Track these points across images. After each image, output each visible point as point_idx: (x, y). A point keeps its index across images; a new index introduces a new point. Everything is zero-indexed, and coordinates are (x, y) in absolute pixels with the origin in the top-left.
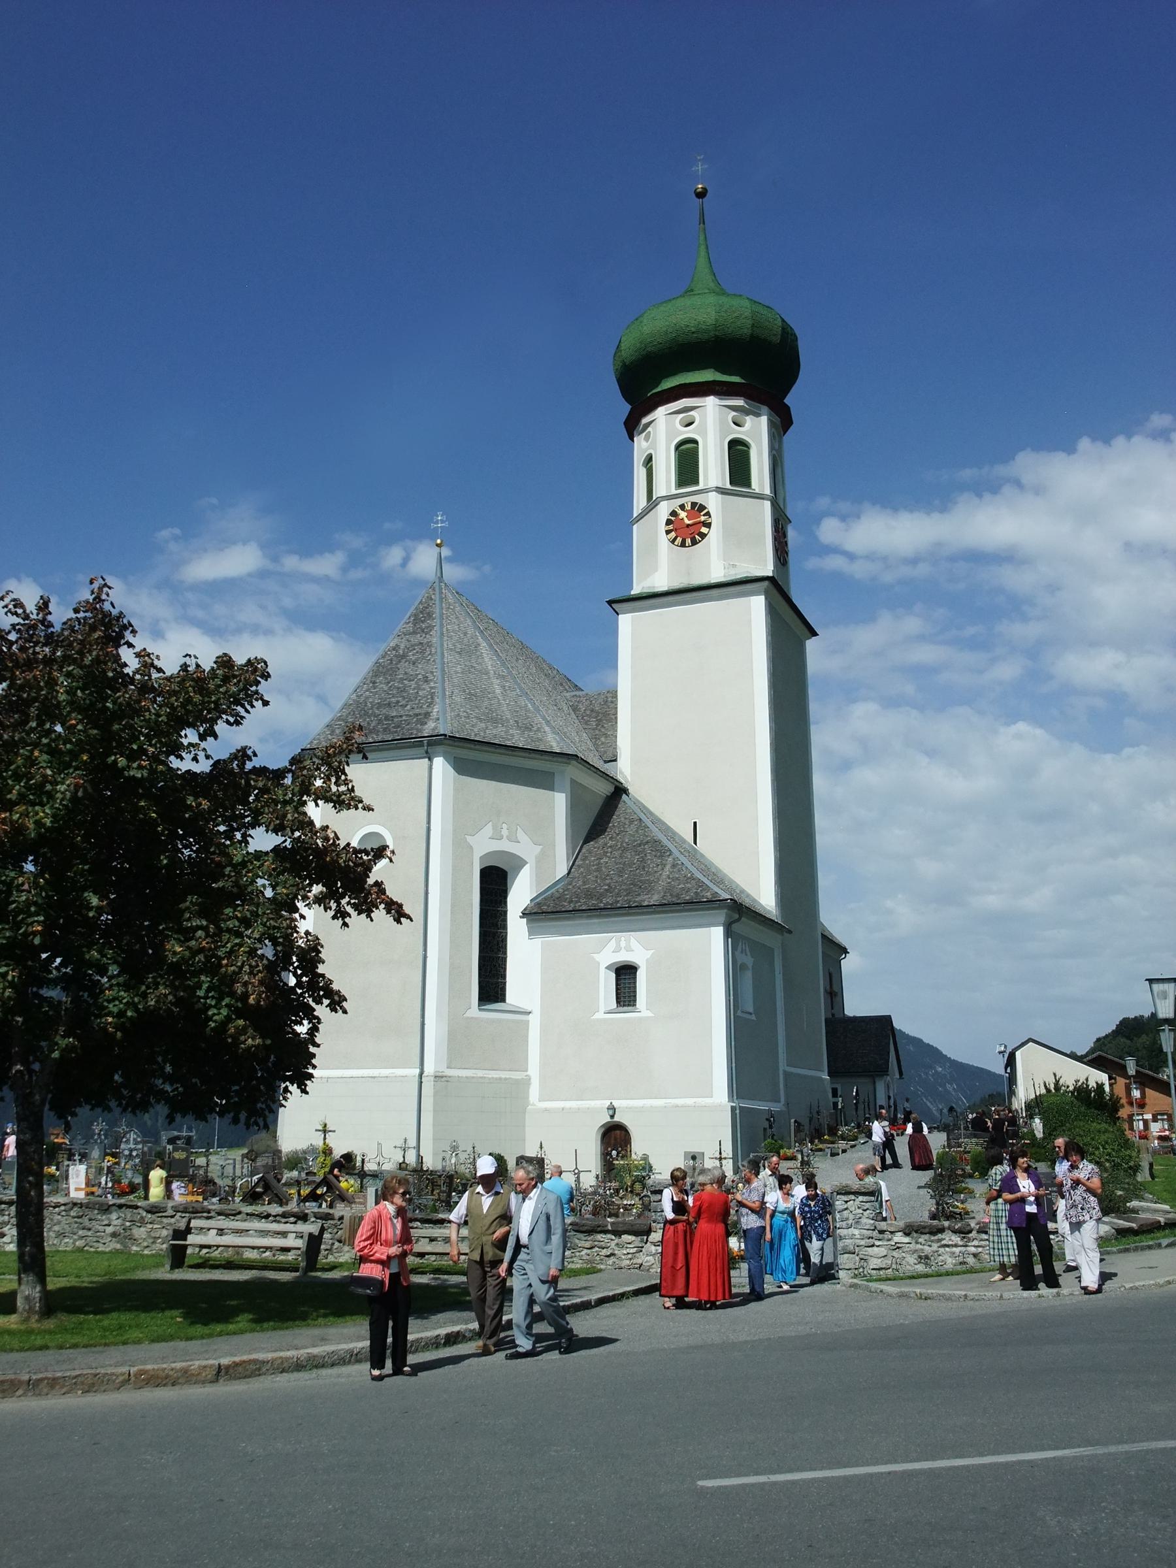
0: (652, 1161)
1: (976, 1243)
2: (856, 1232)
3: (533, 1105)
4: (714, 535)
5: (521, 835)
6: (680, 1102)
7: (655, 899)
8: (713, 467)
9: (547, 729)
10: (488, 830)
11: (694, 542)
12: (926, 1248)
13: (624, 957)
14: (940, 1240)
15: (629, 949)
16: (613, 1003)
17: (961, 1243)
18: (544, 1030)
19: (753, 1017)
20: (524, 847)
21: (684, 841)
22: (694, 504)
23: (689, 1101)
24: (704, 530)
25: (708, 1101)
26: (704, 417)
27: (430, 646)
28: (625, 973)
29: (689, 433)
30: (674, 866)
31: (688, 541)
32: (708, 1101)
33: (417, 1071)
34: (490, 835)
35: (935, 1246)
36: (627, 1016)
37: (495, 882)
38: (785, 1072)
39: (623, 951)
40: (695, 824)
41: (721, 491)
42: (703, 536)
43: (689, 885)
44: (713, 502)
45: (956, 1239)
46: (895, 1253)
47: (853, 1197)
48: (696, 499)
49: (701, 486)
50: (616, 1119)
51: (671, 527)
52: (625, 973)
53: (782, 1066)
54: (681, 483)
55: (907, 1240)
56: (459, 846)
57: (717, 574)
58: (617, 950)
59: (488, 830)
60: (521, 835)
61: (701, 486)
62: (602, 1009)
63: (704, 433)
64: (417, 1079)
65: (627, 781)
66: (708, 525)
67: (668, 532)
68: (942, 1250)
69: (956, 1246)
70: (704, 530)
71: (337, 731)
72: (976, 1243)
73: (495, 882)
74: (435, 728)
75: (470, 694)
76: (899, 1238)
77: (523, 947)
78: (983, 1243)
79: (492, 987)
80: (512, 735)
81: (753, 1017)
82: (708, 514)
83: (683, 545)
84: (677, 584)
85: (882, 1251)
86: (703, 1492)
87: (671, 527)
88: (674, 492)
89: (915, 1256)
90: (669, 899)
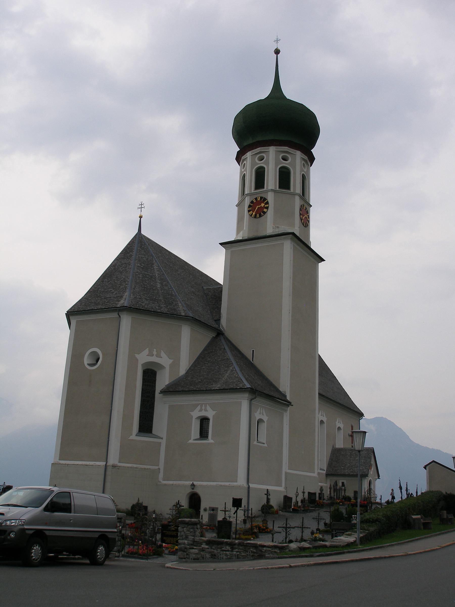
1: (237, 550)
2: (186, 542)
3: (160, 482)
4: (270, 213)
5: (163, 354)
6: (223, 484)
7: (217, 386)
8: (272, 180)
9: (180, 304)
10: (146, 352)
11: (260, 216)
12: (215, 551)
13: (203, 414)
14: (221, 548)
15: (206, 410)
16: (198, 436)
17: (230, 550)
18: (167, 447)
19: (266, 445)
20: (164, 360)
21: (248, 357)
23: (227, 484)
24: (265, 210)
25: (235, 484)
26: (268, 157)
27: (129, 265)
28: (204, 421)
29: (261, 164)
30: (232, 371)
31: (258, 215)
32: (235, 484)
33: (105, 463)
34: (147, 354)
35: (219, 550)
37: (150, 375)
38: (286, 473)
39: (203, 411)
40: (253, 351)
41: (272, 190)
42: (264, 213)
43: (235, 381)
44: (270, 197)
45: (228, 548)
46: (202, 553)
47: (186, 526)
48: (263, 195)
50: (194, 490)
51: (251, 209)
52: (204, 421)
53: (285, 468)
54: (257, 188)
55: (207, 547)
56: (132, 360)
57: (270, 231)
58: (201, 410)
59: (146, 352)
60: (163, 354)
62: (193, 437)
64: (104, 467)
65: (224, 329)
66: (267, 208)
67: (249, 211)
68: (222, 552)
69: (228, 551)
70: (265, 210)
71: (83, 304)
72: (237, 550)
73: (150, 375)
74: (124, 303)
75: (144, 287)
76: (204, 546)
77: (162, 409)
78: (240, 550)
79: (146, 426)
80: (162, 307)
81: (266, 445)
82: (267, 203)
83: (255, 217)
84: (251, 236)
85: (196, 551)
87: (251, 209)
89: (210, 554)
90: (225, 387)
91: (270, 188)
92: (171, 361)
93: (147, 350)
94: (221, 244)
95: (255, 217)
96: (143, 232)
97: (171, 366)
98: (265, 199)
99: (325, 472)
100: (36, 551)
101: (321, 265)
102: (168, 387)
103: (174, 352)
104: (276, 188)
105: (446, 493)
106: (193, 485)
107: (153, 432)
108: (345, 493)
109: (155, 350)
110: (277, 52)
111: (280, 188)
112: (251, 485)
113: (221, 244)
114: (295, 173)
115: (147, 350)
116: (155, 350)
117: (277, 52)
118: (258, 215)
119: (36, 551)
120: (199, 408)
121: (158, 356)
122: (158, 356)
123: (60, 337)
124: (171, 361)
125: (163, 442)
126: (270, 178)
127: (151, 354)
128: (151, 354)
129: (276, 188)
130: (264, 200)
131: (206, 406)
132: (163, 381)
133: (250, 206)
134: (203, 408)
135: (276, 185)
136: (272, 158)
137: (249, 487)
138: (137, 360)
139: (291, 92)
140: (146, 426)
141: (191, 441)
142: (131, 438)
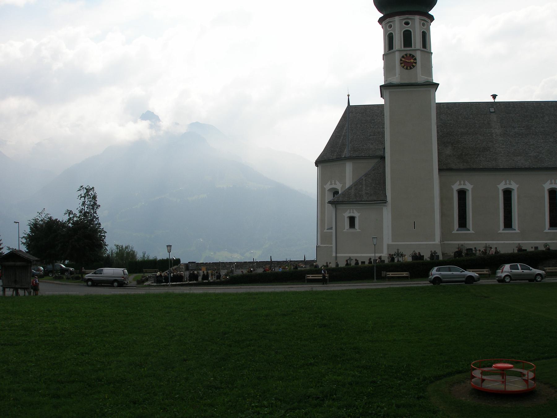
0: (120, 244)
5: (337, 182)
10: (329, 183)
11: (411, 68)
22: (410, 55)
24: (414, 64)
25: (434, 243)
28: (352, 220)
29: (407, 28)
31: (409, 68)
36: (352, 230)
42: (414, 66)
49: (413, 48)
52: (352, 220)
54: (405, 46)
58: (350, 213)
59: (329, 183)
60: (337, 182)
61: (413, 48)
63: (395, 31)
66: (416, 63)
70: (414, 64)
82: (415, 59)
83: (407, 69)
86: (511, 363)
88: (403, 48)
91: (396, 49)
92: (472, 186)
98: (413, 56)
100: (116, 284)
104: (401, 48)
105: (419, 253)
108: (336, 253)
111: (404, 47)
112: (338, 255)
119: (116, 284)
121: (464, 184)
123: (312, 173)
124: (472, 186)
127: (506, 184)
128: (506, 184)
129: (401, 48)
130: (412, 57)
137: (336, 257)
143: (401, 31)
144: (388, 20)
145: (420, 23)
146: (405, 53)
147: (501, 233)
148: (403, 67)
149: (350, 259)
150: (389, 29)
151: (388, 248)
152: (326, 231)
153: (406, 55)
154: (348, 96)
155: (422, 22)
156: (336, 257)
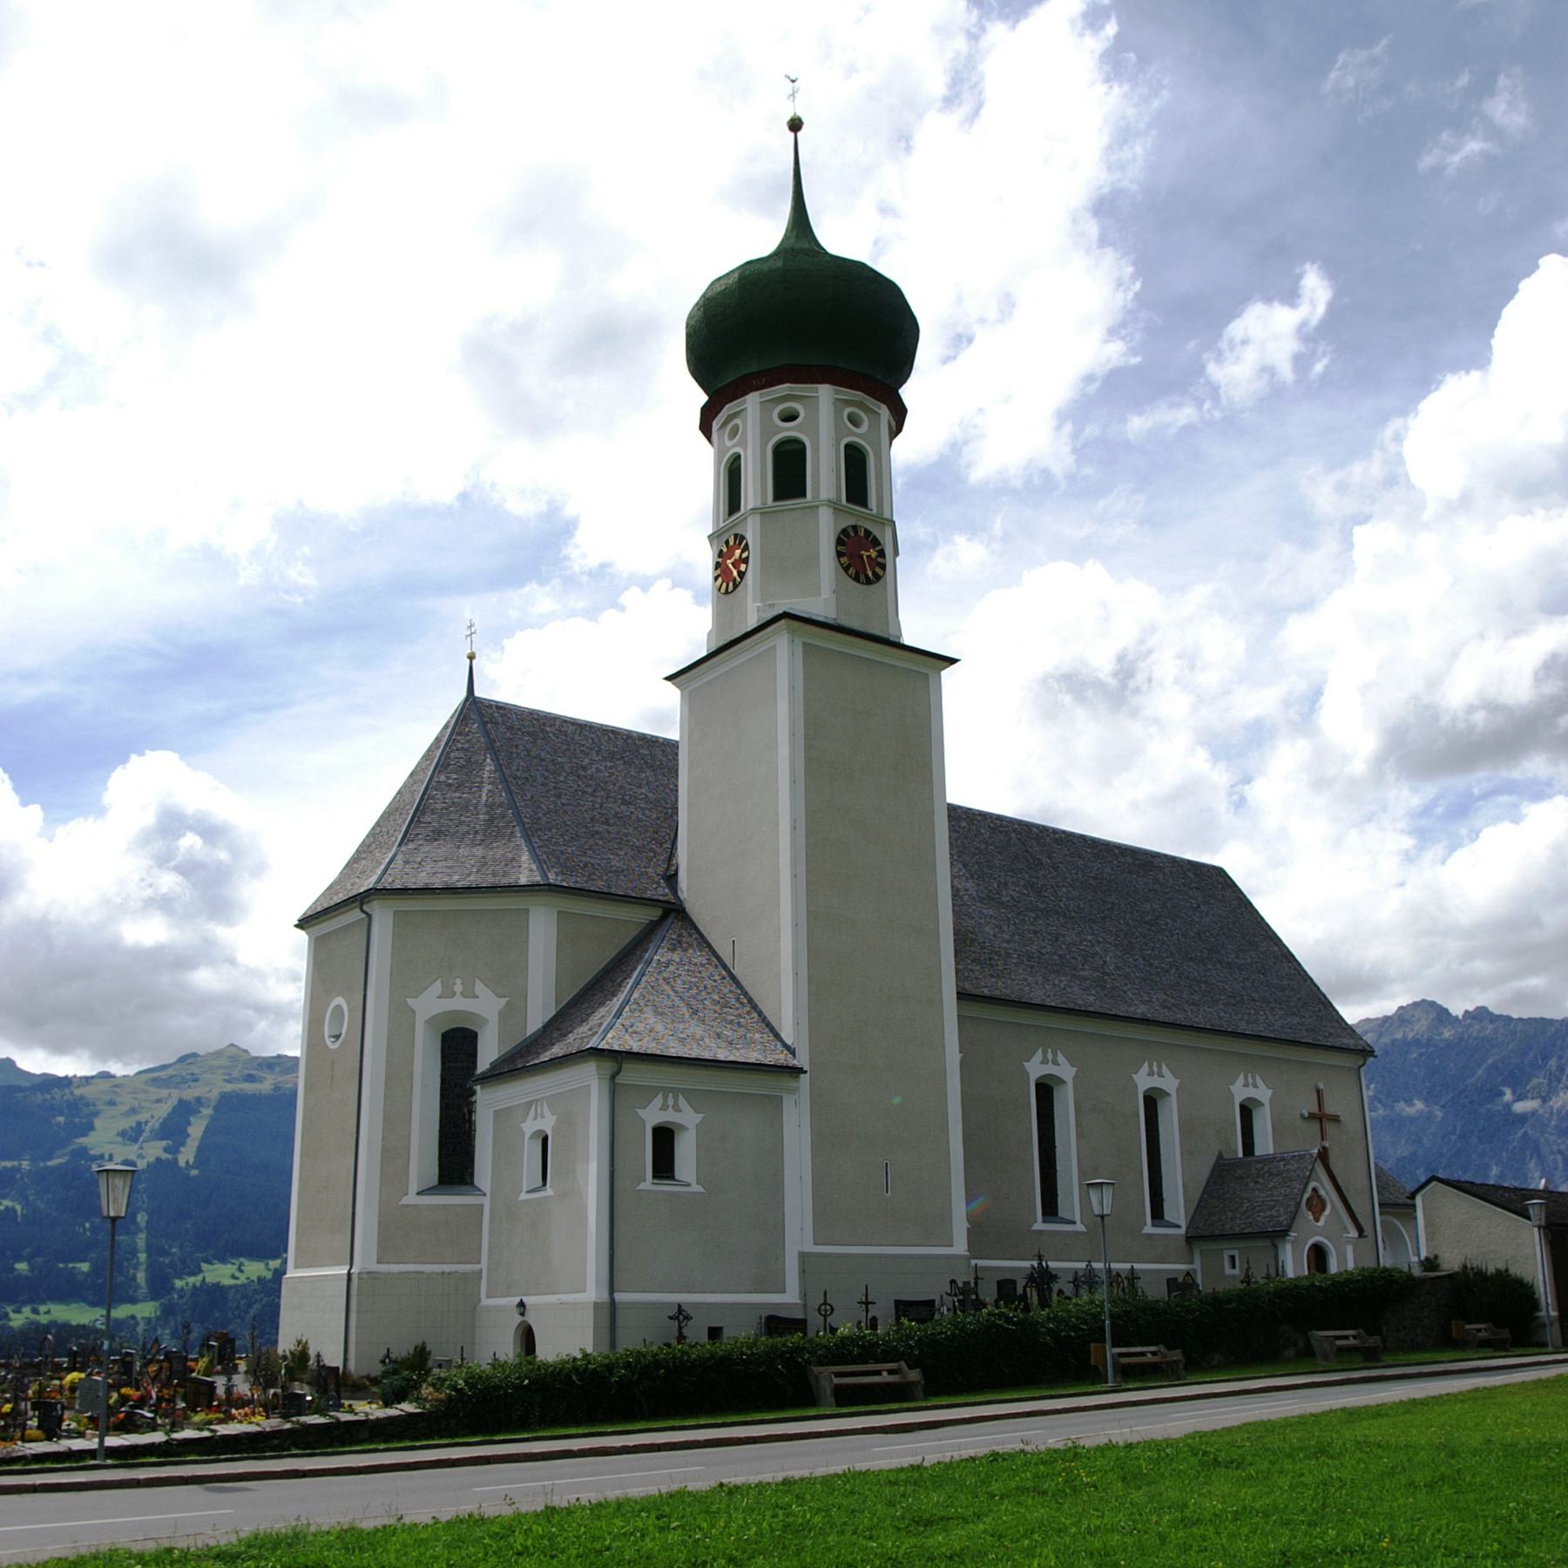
5: (480, 988)
15: (677, 1109)
29: (789, 431)
31: (878, 570)
36: (665, 1187)
37: (458, 1045)
56: (401, 1016)
58: (664, 1108)
59: (1039, 1055)
60: (1165, 1069)
79: (456, 1166)
81: (700, 1189)
91: (751, 505)
93: (438, 983)
94: (669, 678)
95: (727, 592)
96: (478, 693)
97: (504, 1015)
99: (1182, 1231)
101: (947, 675)
102: (494, 1065)
103: (510, 982)
106: (521, 1304)
107: (677, 1175)
108: (612, 1291)
109: (458, 981)
110: (795, 125)
111: (777, 497)
112: (618, 1296)
113: (669, 678)
114: (816, 448)
115: (438, 983)
116: (458, 981)
117: (795, 125)
118: (878, 570)
120: (659, 1100)
121: (469, 993)
122: (469, 993)
125: (486, 1201)
126: (750, 477)
127: (448, 993)
128: (448, 993)
131: (676, 1099)
132: (488, 1054)
133: (839, 542)
134: (671, 1101)
135: (764, 493)
136: (822, 416)
137: (613, 1302)
138: (414, 1012)
139: (839, 237)
140: (456, 1166)
141: (523, 1196)
142: (405, 1201)
143: (764, 444)
144: (727, 410)
145: (838, 413)
146: (850, 521)
147: (1041, 1232)
148: (846, 569)
149: (681, 1314)
150: (728, 443)
151: (803, 1272)
152: (411, 1199)
153: (855, 528)
154: (471, 657)
155: (847, 411)
156: (613, 1302)
